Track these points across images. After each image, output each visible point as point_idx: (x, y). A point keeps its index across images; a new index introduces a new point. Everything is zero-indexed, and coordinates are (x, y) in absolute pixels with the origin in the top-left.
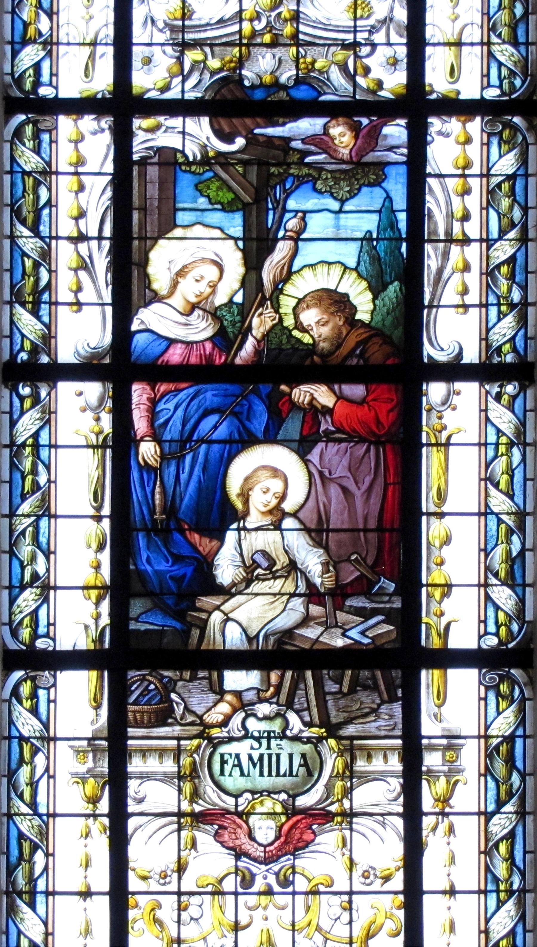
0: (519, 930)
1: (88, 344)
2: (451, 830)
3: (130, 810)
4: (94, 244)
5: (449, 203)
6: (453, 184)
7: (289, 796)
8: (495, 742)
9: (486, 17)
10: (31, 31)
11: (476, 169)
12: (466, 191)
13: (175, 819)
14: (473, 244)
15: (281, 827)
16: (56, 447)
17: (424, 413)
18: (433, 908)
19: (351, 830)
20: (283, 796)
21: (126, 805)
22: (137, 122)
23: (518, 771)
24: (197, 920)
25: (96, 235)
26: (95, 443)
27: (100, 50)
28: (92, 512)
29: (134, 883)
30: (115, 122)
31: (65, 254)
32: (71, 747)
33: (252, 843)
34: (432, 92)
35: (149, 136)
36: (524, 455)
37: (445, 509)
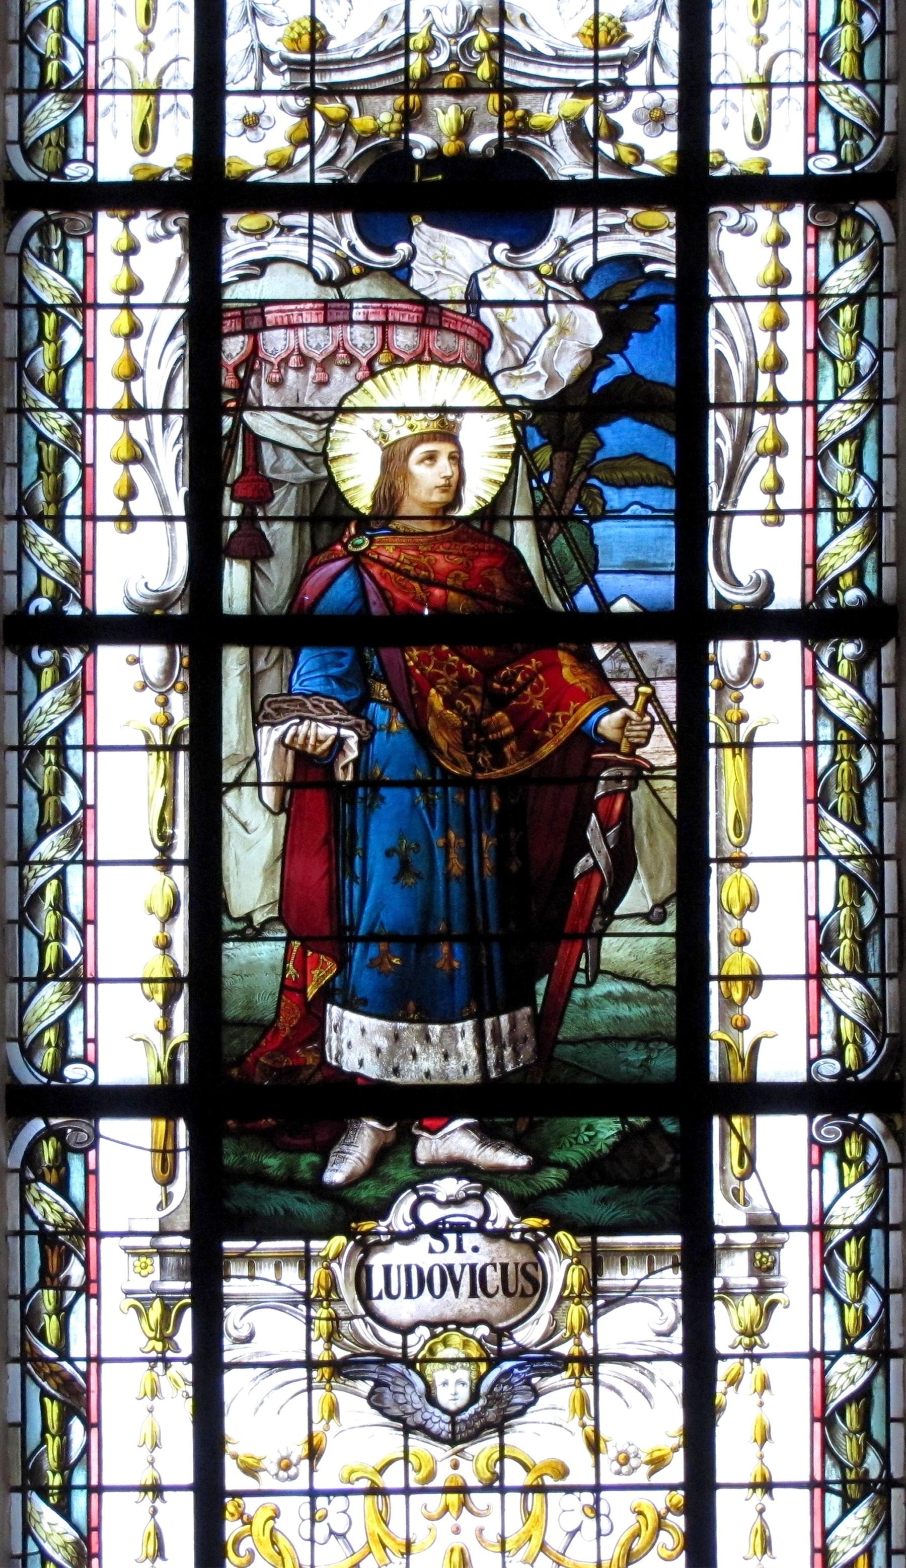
0: (880, 1546)
1: (146, 585)
2: (766, 1385)
3: (227, 1357)
4: (157, 419)
5: (751, 342)
6: (760, 313)
7: (493, 1329)
8: (838, 1236)
9: (812, 40)
10: (52, 73)
11: (796, 287)
12: (780, 324)
13: (302, 1372)
14: (791, 409)
15: (481, 1378)
16: (96, 748)
17: (712, 693)
18: (732, 1513)
19: (596, 1383)
20: (483, 1330)
21: (220, 1350)
22: (232, 220)
23: (877, 1286)
24: (343, 1536)
25: (160, 406)
26: (160, 742)
27: (166, 101)
28: (154, 854)
29: (233, 1479)
30: (191, 221)
31: (107, 436)
32: (125, 1249)
33: (431, 1409)
34: (720, 165)
35: (252, 242)
36: (878, 760)
37: (749, 850)
